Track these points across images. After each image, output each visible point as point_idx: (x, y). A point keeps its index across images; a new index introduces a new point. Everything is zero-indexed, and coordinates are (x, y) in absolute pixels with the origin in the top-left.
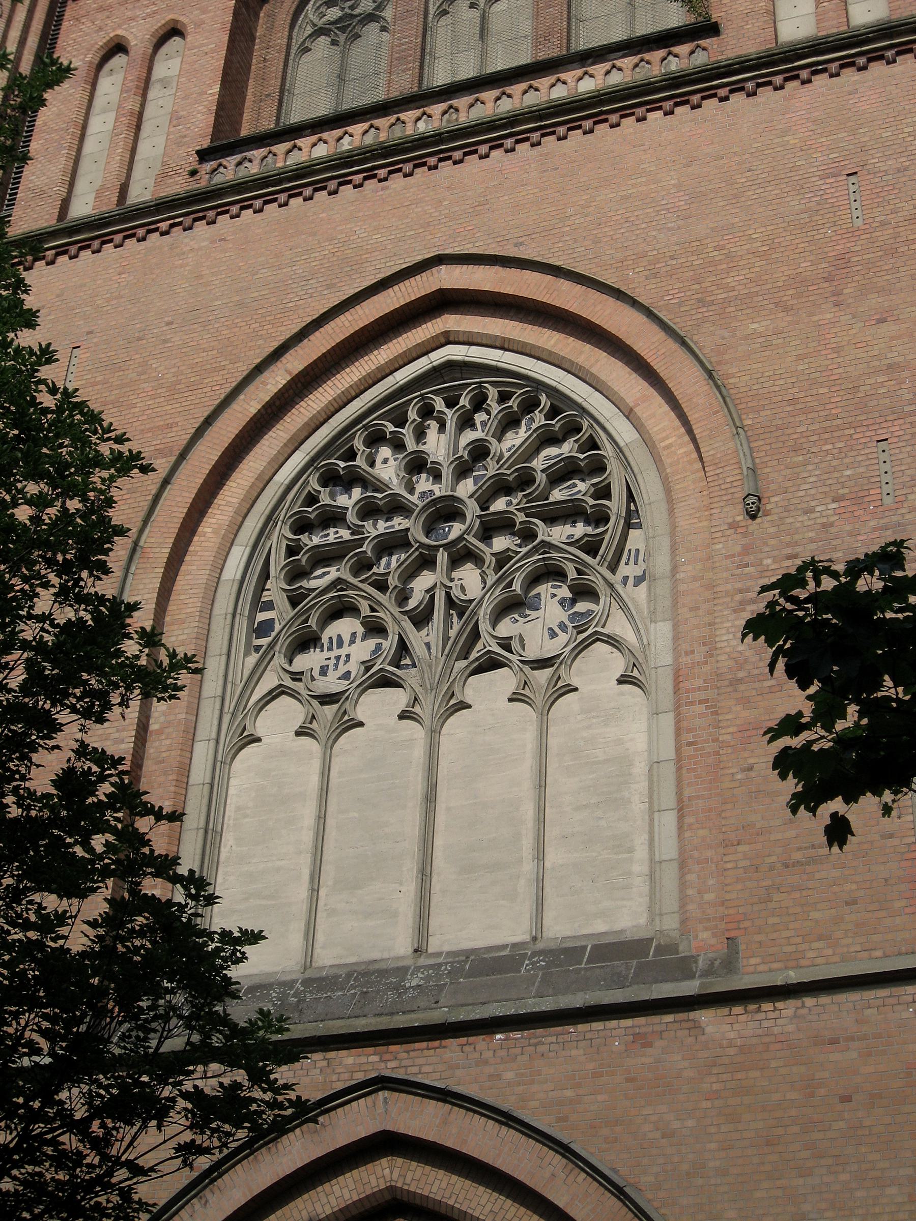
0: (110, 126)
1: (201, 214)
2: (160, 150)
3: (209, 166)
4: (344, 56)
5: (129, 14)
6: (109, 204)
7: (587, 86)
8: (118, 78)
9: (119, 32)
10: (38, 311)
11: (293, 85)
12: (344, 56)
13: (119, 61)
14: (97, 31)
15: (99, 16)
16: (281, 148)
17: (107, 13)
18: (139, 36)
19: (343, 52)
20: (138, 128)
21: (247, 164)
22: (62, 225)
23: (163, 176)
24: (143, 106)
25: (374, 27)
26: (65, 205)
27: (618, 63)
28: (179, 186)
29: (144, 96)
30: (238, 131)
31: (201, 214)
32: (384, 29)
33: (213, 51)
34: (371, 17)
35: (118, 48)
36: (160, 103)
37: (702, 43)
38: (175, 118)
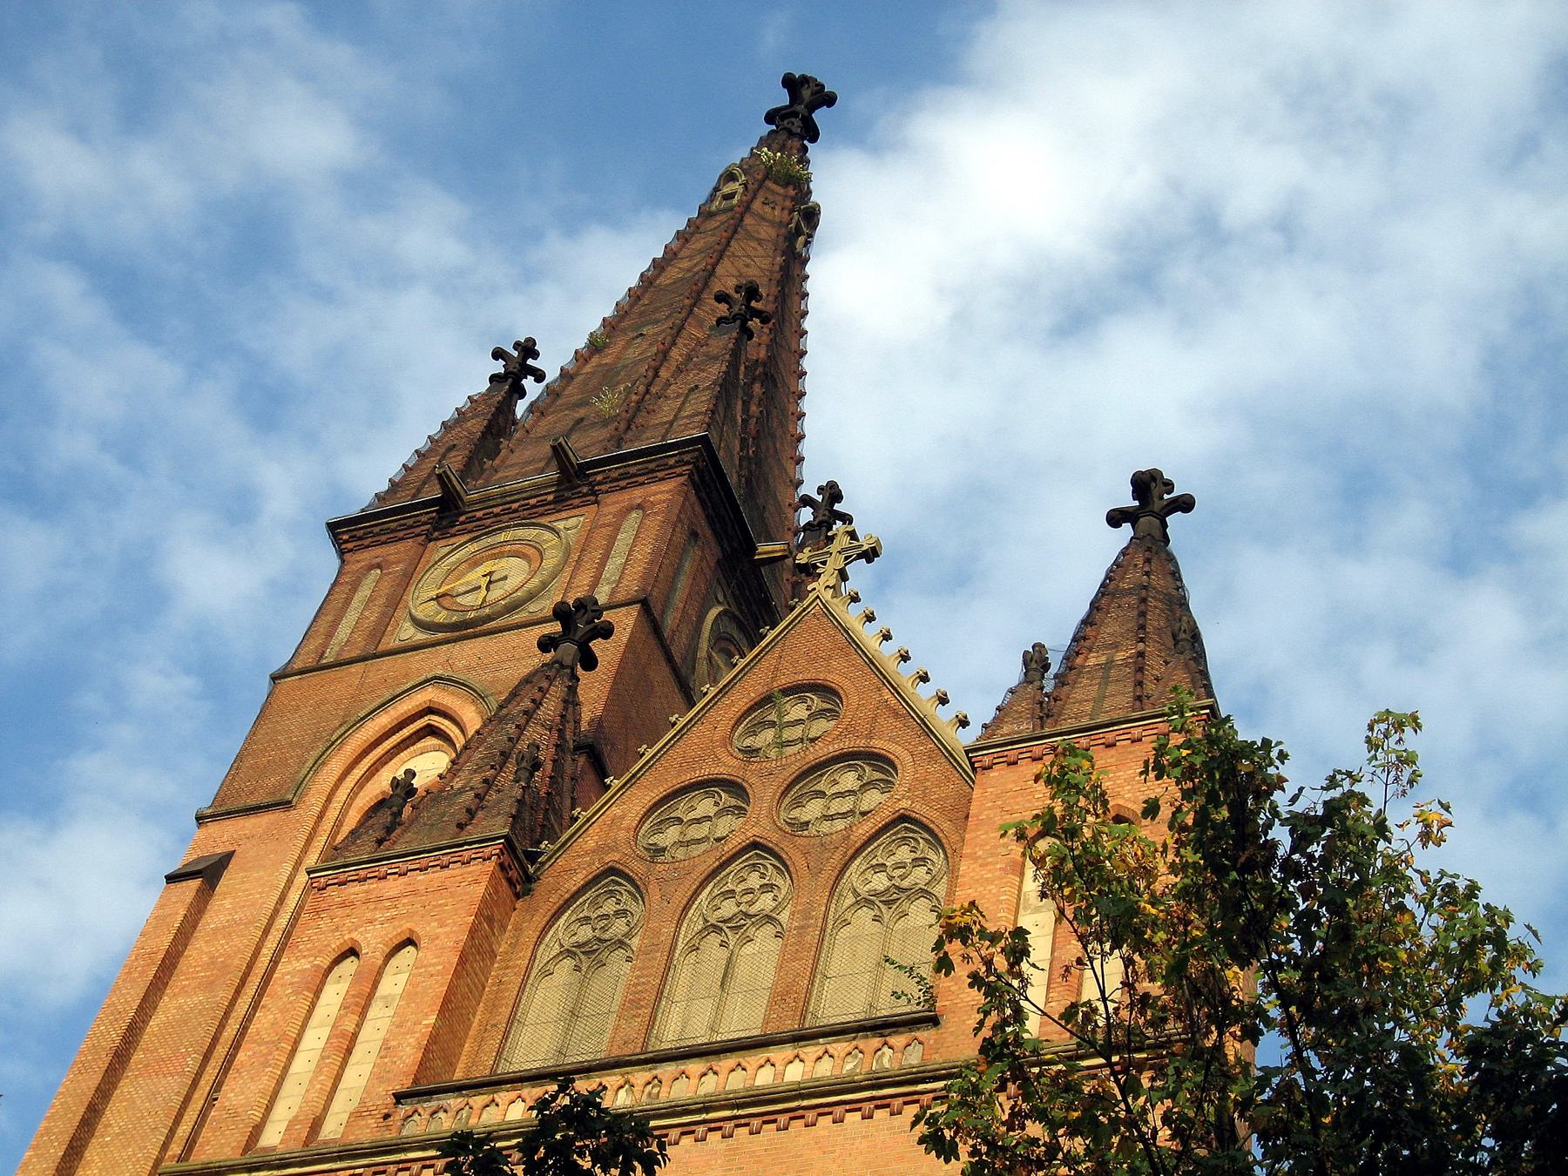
0: (322, 1043)
1: (381, 1168)
2: (363, 1082)
3: (404, 1109)
4: (583, 985)
5: (369, 915)
6: (295, 1148)
7: (795, 1074)
8: (343, 987)
9: (355, 935)
10: (1186, 504)
11: (525, 1014)
12: (583, 985)
13: (350, 965)
14: (333, 931)
15: (340, 912)
16: (478, 1100)
17: (348, 911)
18: (372, 941)
19: (581, 983)
20: (349, 1051)
21: (441, 1114)
22: (250, 1158)
23: (357, 1115)
24: (359, 1026)
25: (769, 929)
26: (257, 1130)
27: (831, 1049)
28: (367, 1133)
29: (363, 1015)
30: (452, 1066)
31: (381, 1168)
32: (629, 959)
33: (439, 973)
34: (621, 944)
35: (353, 952)
36: (379, 1020)
37: (917, 1034)
38: (386, 1047)
